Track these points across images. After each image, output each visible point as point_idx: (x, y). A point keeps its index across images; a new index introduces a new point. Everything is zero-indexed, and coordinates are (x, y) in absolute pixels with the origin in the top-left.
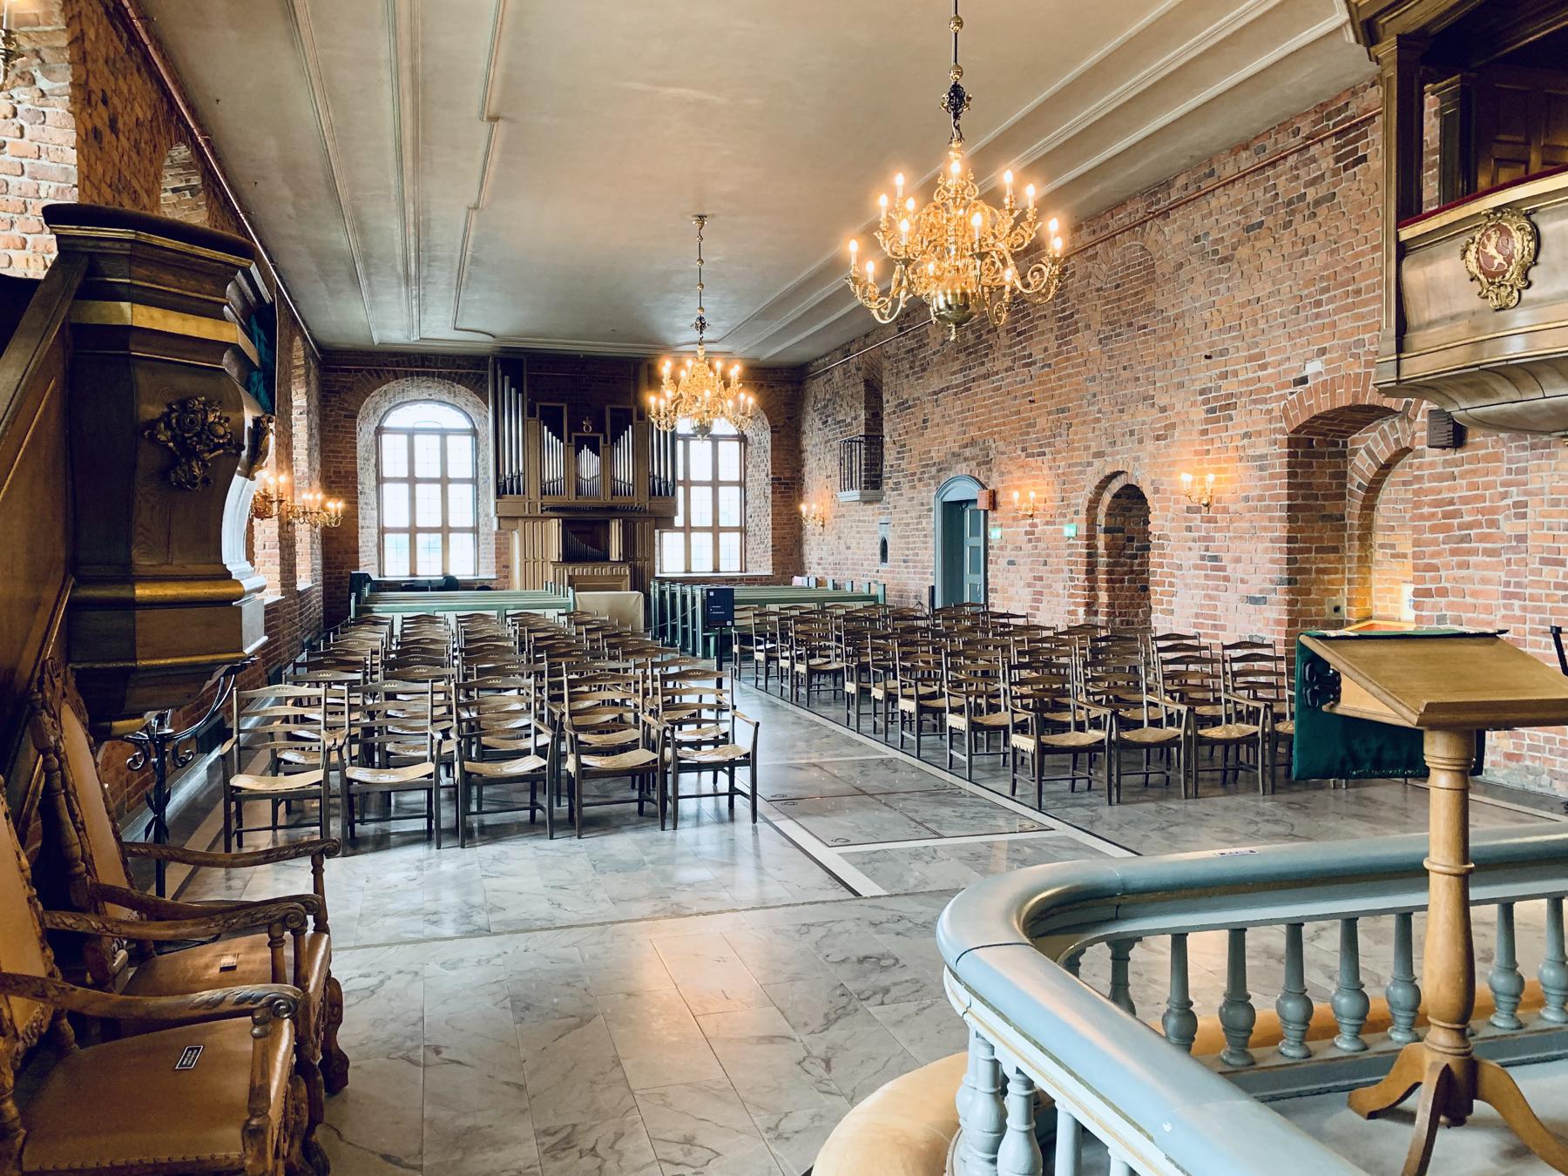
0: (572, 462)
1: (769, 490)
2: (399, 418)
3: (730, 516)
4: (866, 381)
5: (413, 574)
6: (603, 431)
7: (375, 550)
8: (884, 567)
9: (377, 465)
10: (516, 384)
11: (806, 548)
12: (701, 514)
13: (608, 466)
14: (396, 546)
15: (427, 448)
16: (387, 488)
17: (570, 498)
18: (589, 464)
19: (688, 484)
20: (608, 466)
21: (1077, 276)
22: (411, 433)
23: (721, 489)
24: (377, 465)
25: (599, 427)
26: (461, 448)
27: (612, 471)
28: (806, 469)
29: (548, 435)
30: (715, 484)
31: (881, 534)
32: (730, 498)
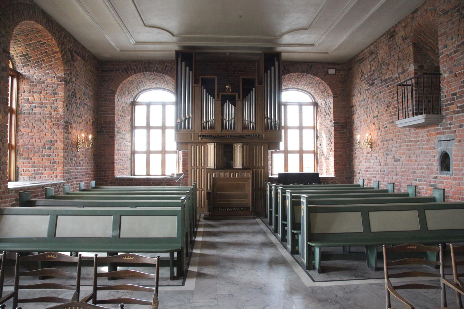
0: (220, 113)
1: (332, 129)
2: (143, 97)
3: (309, 145)
4: (415, 45)
5: (148, 175)
6: (238, 92)
7: (129, 162)
8: (445, 175)
9: (131, 120)
10: (212, 93)
11: (356, 162)
12: (293, 145)
13: (241, 113)
14: (140, 160)
15: (156, 111)
16: (137, 131)
17: (219, 131)
18: (230, 111)
19: (286, 128)
20: (241, 113)
21: (362, 115)
22: (148, 105)
23: (290, 155)
24: (131, 120)
25: (235, 88)
26: (171, 111)
27: (243, 116)
28: (356, 116)
29: (206, 96)
30: (301, 128)
31: (441, 148)
32: (309, 135)
